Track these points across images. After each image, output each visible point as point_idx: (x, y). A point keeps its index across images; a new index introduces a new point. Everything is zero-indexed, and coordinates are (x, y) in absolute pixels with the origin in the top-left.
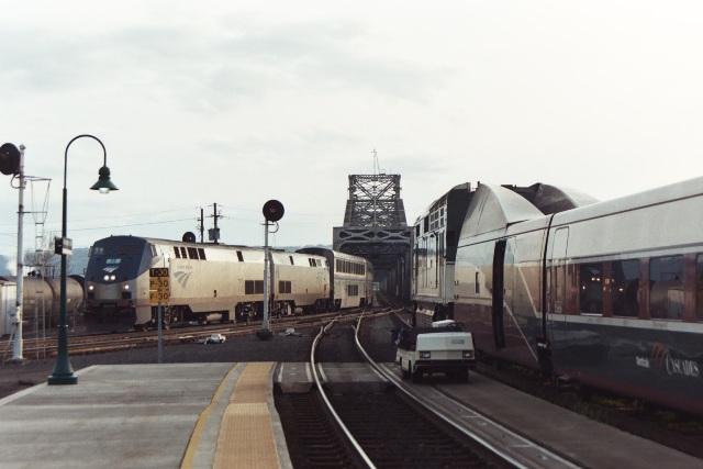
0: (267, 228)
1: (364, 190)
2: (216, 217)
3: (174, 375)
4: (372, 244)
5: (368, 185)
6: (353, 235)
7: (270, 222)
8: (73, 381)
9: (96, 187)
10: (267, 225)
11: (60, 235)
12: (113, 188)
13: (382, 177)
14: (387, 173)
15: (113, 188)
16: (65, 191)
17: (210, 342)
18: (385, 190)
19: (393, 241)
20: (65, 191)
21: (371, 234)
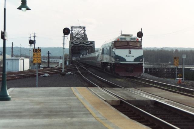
0: (64, 37)
1: (75, 31)
2: (34, 37)
3: (51, 94)
4: (81, 46)
5: (76, 29)
6: (87, 43)
7: (65, 35)
8: (8, 99)
9: (20, 8)
10: (64, 36)
11: (3, 31)
12: (28, 9)
13: (80, 27)
14: (82, 26)
15: (28, 9)
16: (5, 9)
17: (44, 76)
18: (81, 31)
19: (87, 45)
20: (5, 9)
21: (81, 43)
